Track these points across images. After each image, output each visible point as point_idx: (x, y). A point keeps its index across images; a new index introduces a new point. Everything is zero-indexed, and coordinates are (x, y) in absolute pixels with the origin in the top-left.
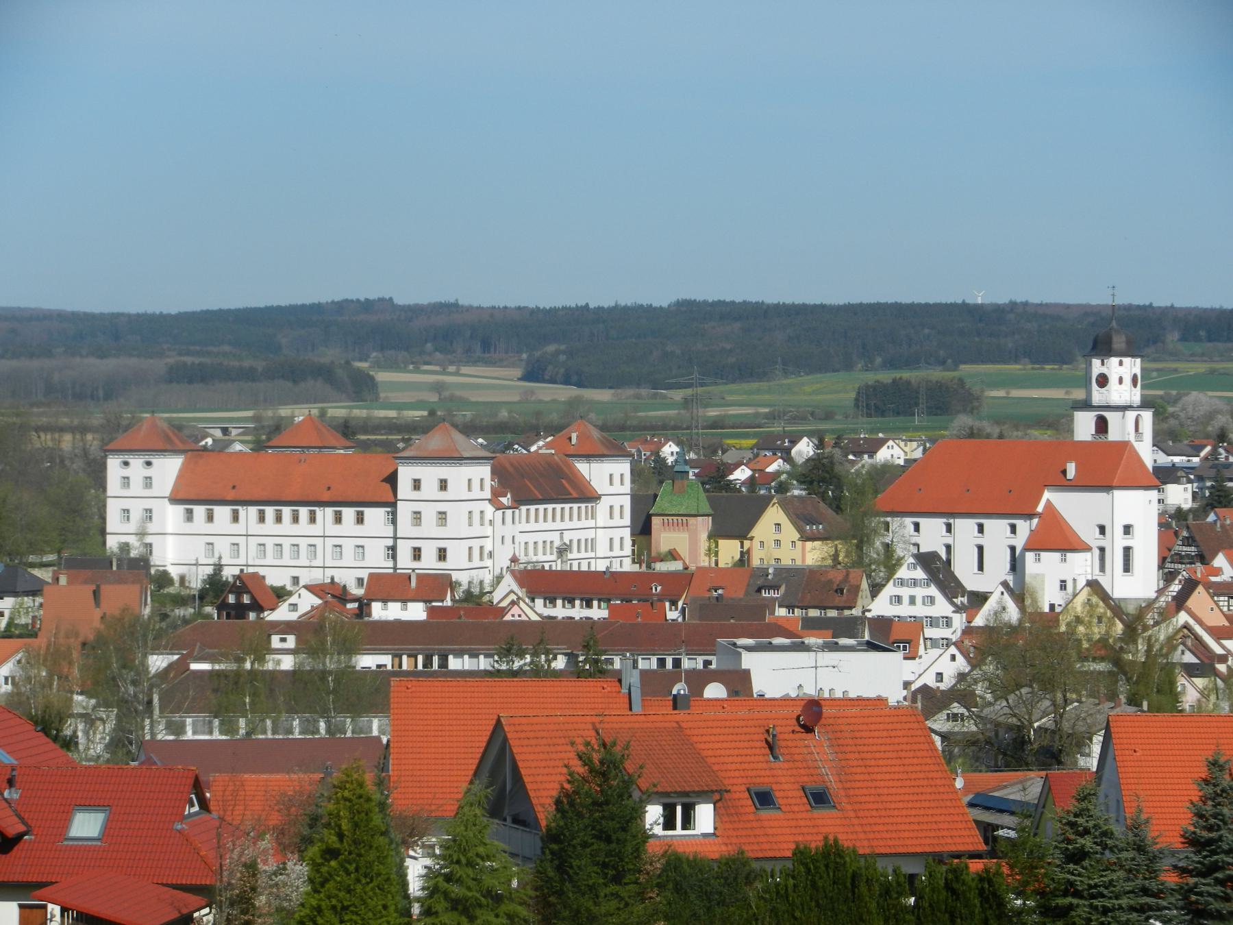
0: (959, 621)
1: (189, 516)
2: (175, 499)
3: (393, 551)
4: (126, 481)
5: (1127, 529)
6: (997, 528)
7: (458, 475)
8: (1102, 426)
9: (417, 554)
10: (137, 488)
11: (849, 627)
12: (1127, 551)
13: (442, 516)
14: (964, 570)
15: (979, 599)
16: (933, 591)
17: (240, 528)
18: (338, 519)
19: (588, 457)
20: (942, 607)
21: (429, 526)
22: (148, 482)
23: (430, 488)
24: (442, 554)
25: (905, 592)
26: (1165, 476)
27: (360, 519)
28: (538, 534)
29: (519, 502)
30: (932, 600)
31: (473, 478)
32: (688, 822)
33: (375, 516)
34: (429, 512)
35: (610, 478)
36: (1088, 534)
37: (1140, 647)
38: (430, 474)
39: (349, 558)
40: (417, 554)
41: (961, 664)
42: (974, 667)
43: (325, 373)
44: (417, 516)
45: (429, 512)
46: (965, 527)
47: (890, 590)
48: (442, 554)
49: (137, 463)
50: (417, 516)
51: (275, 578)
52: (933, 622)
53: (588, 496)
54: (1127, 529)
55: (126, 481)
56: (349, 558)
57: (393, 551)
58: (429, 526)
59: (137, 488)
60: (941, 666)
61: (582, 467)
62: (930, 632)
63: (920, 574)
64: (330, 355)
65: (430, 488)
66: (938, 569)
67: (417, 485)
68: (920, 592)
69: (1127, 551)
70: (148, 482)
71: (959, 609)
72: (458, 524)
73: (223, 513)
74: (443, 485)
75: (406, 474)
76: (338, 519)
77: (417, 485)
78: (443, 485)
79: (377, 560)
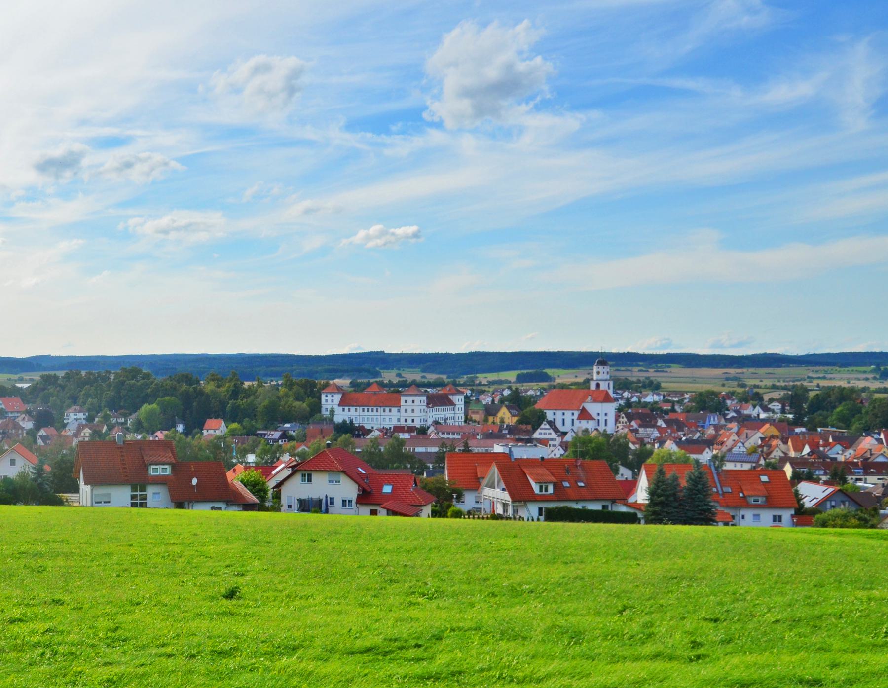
0: (559, 440)
1: (344, 410)
2: (340, 405)
3: (399, 420)
4: (326, 401)
5: (606, 414)
6: (568, 414)
7: (417, 399)
8: (598, 385)
9: (406, 421)
10: (329, 402)
11: (530, 441)
12: (606, 420)
13: (413, 411)
14: (559, 424)
15: (565, 433)
16: (551, 431)
17: (357, 413)
18: (384, 411)
19: (453, 394)
20: (554, 435)
21: (409, 413)
22: (332, 401)
23: (410, 402)
24: (413, 421)
25: (543, 431)
26: (616, 400)
27: (390, 411)
28: (439, 413)
29: (433, 407)
30: (550, 434)
31: (421, 401)
32: (546, 490)
33: (394, 410)
34: (409, 410)
35: (458, 400)
36: (594, 415)
37: (158, 433)
38: (409, 399)
39: (387, 422)
40: (406, 421)
41: (562, 452)
42: (565, 451)
43: (368, 371)
44: (406, 411)
45: (409, 410)
46: (559, 413)
47: (539, 431)
48: (413, 421)
49: (329, 396)
50: (406, 411)
51: (367, 427)
52: (552, 440)
53: (452, 404)
54: (606, 414)
55: (326, 401)
56: (387, 422)
57: (399, 420)
58: (409, 413)
59: (329, 402)
60: (559, 452)
61: (451, 397)
62: (550, 443)
63: (547, 426)
64: (366, 366)
65: (410, 402)
66: (552, 424)
67: (406, 402)
68: (548, 431)
69: (606, 420)
70: (332, 401)
71: (559, 436)
72: (414, 410)
73: (381, 409)
74: (413, 402)
75: (403, 399)
76: (384, 411)
77: (406, 402)
78: (413, 402)
79: (395, 422)
